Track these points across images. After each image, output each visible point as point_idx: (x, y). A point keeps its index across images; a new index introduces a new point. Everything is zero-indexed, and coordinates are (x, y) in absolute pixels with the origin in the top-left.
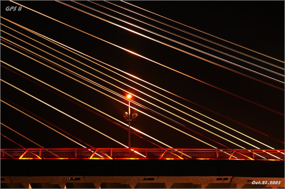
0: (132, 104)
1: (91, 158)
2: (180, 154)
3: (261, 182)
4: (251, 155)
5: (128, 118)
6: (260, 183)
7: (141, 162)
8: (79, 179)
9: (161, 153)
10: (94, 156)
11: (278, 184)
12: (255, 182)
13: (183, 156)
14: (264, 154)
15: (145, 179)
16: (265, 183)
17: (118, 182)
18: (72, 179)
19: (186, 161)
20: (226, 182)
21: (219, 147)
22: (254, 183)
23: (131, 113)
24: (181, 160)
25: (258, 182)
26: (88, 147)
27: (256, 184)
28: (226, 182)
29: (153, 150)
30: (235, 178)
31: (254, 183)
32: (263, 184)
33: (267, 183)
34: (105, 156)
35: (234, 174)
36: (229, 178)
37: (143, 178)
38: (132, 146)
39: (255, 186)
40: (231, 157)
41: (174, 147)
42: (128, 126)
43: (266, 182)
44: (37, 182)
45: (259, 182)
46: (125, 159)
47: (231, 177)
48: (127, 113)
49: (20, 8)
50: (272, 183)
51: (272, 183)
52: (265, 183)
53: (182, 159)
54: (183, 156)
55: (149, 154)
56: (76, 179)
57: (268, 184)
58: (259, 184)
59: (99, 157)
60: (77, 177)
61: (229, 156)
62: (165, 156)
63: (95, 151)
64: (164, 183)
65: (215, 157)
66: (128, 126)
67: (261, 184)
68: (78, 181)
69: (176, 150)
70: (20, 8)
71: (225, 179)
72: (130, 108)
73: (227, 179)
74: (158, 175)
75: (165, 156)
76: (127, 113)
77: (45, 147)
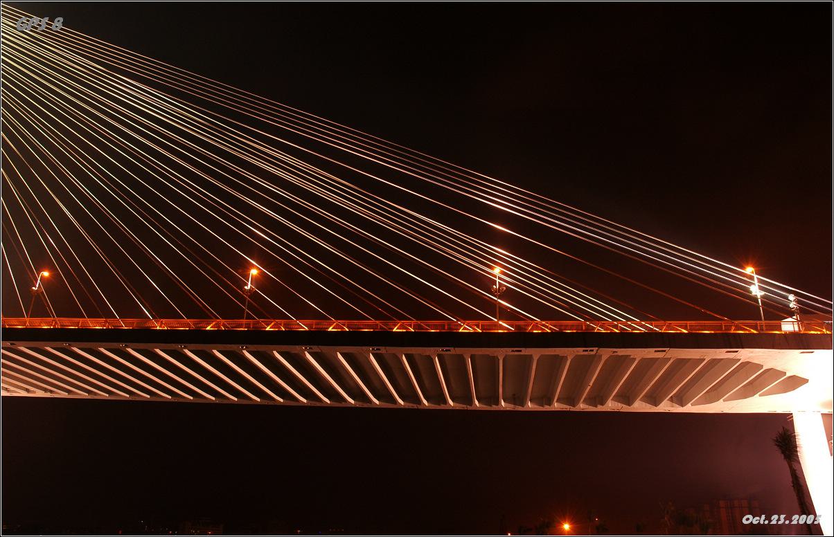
0: (500, 278)
1: (460, 331)
2: (547, 327)
3: (768, 518)
4: (616, 327)
5: (496, 292)
6: (764, 521)
7: (509, 334)
8: (449, 350)
9: (529, 325)
10: (465, 329)
11: (813, 522)
12: (750, 516)
13: (550, 329)
14: (630, 326)
15: (513, 351)
16: (779, 520)
17: (488, 353)
18: (442, 350)
19: (553, 333)
20: (592, 353)
21: (586, 320)
22: (748, 519)
23: (499, 288)
24: (548, 332)
25: (760, 517)
26: (458, 320)
27: (755, 522)
28: (592, 353)
29: (521, 323)
30: (601, 349)
31: (748, 519)
32: (774, 522)
33: (785, 519)
34: (474, 329)
35: (600, 346)
36: (595, 349)
37: (511, 349)
38: (499, 319)
39: (753, 529)
40: (598, 329)
41: (542, 320)
42: (496, 299)
43: (782, 517)
44: (409, 352)
45: (763, 517)
46: (496, 331)
47: (597, 348)
48: (495, 286)
49: (59, 21)
50: (798, 520)
51: (798, 520)
52: (779, 520)
53: (549, 331)
54: (550, 329)
55: (517, 327)
56: (447, 350)
57: (787, 522)
58: (762, 522)
59: (468, 329)
60: (448, 348)
61: (594, 328)
62: (532, 329)
63: (464, 323)
64: (531, 355)
65: (582, 329)
66: (496, 299)
67: (766, 522)
68: (448, 352)
69: (544, 323)
70: (59, 21)
71: (590, 351)
72: (24, 317)
73: (593, 351)
74: (526, 346)
75: (532, 329)
76: (495, 286)
77: (417, 320)
